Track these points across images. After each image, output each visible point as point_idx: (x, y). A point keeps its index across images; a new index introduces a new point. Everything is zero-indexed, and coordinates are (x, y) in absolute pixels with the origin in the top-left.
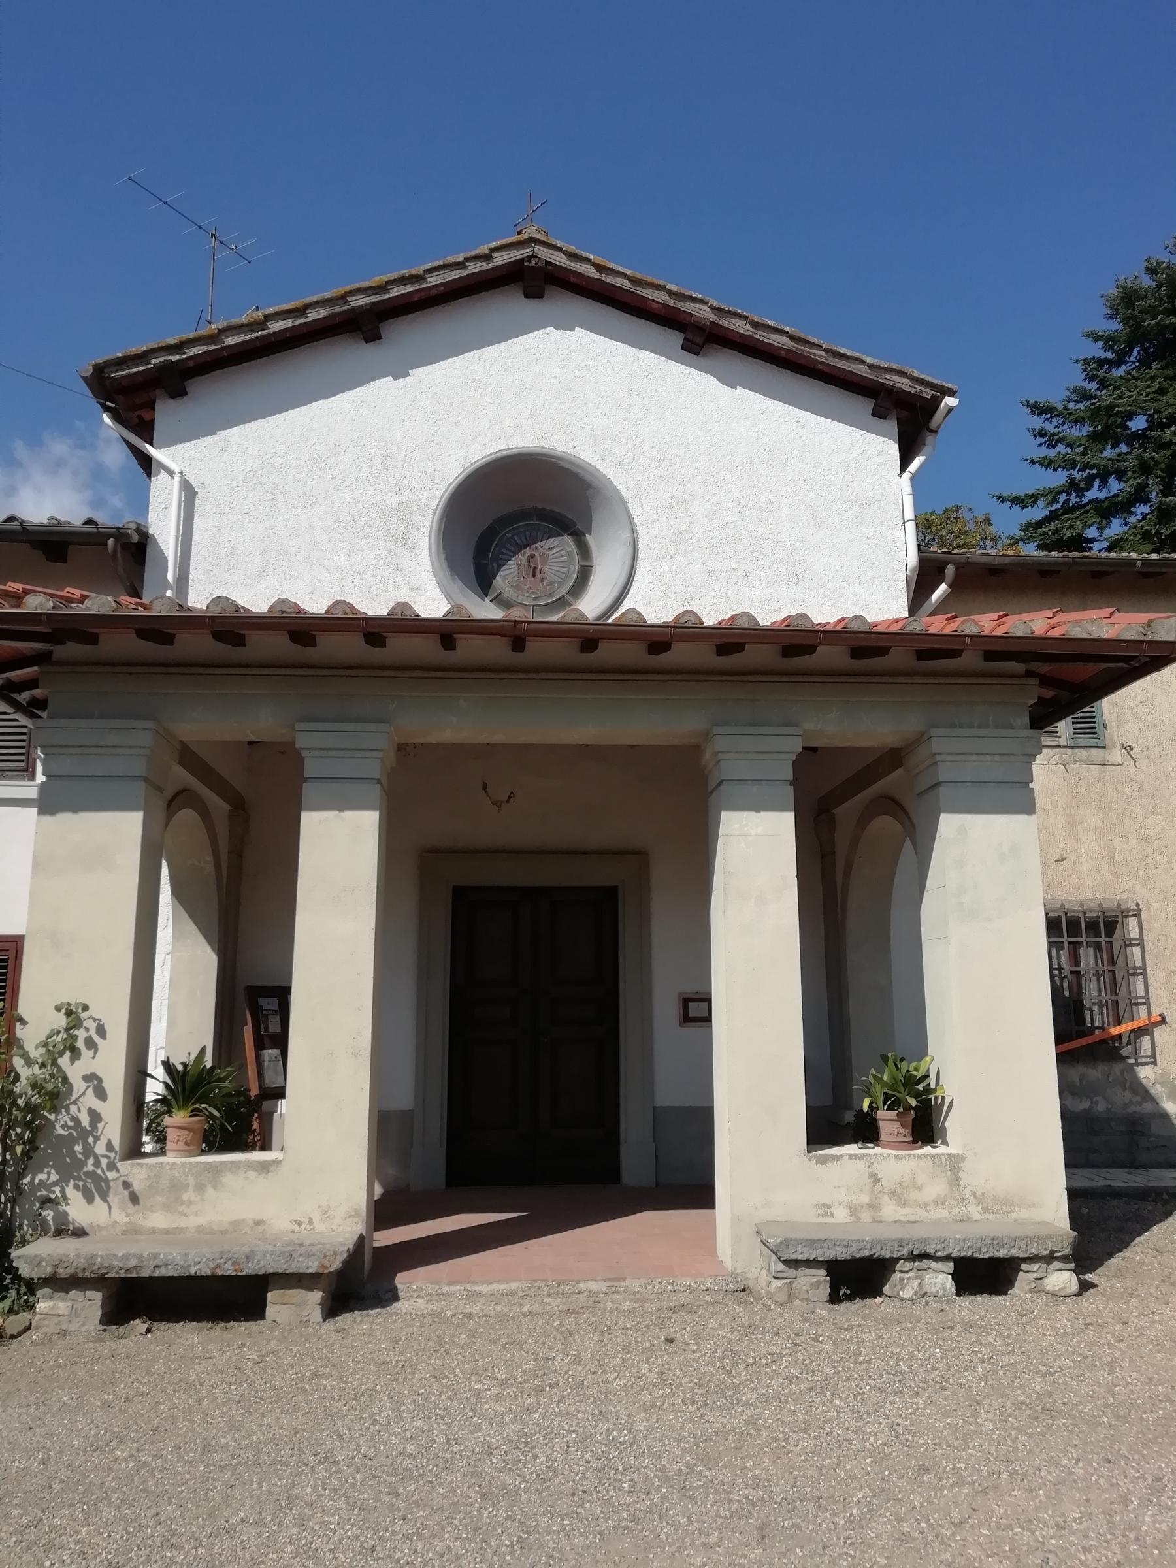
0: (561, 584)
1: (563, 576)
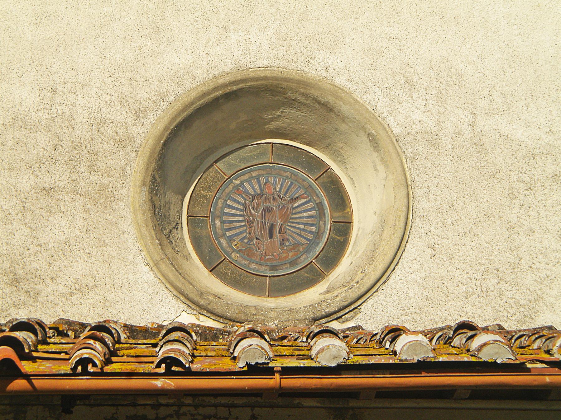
1: (310, 237)
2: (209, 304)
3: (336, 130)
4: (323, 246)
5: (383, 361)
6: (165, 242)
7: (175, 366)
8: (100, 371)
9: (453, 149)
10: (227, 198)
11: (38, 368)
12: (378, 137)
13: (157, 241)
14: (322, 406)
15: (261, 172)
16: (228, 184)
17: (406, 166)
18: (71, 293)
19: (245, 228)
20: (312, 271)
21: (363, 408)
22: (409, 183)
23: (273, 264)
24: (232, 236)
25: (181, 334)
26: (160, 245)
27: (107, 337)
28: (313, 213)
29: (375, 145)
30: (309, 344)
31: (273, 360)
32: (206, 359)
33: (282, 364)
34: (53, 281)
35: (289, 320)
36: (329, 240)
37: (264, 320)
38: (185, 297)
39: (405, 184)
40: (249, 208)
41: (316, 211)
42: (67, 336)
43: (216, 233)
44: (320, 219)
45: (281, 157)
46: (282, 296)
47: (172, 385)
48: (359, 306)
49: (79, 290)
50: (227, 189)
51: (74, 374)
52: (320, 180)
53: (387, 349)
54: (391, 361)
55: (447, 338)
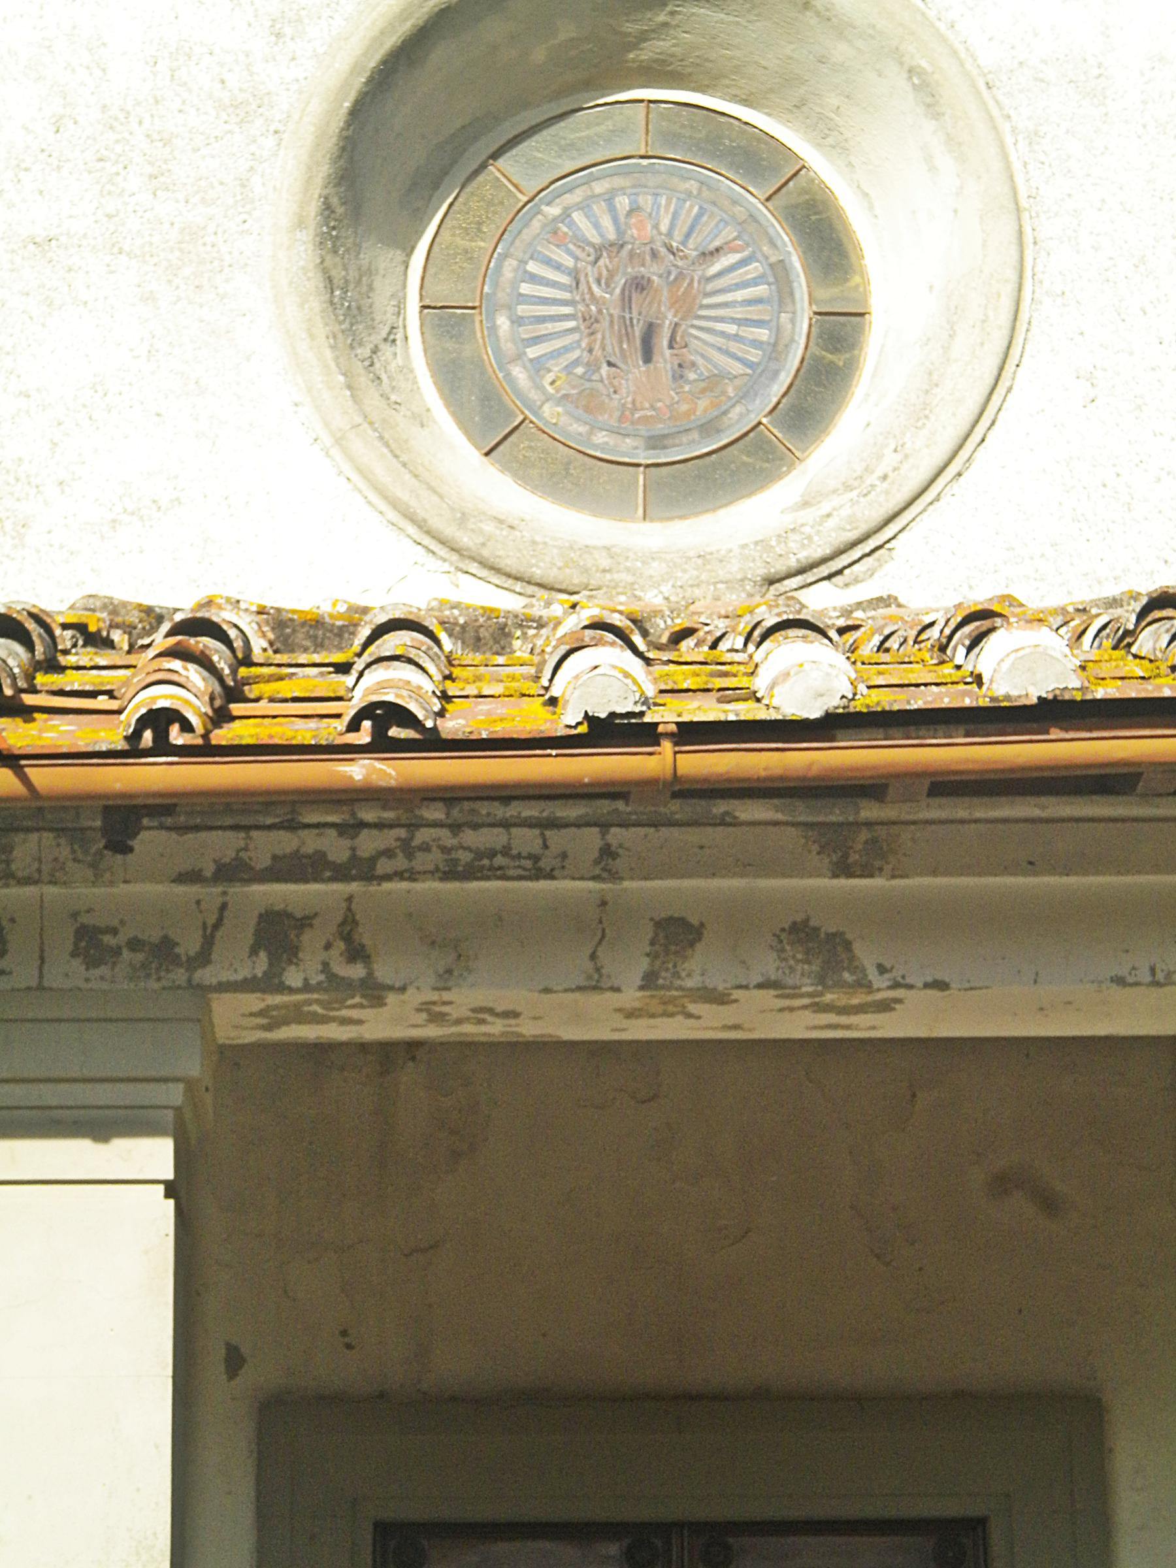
1: (755, 355)
2: (483, 544)
3: (821, 61)
4: (789, 381)
5: (946, 703)
6: (363, 379)
7: (398, 726)
8: (200, 741)
9: (1144, 102)
10: (527, 256)
11: (40, 738)
12: (936, 76)
13: (341, 378)
14: (790, 819)
15: (618, 182)
16: (528, 217)
17: (1013, 157)
18: (114, 521)
19: (576, 336)
20: (761, 448)
21: (894, 823)
22: (1024, 203)
23: (657, 433)
24: (544, 358)
25: (413, 639)
26: (349, 387)
27: (217, 651)
28: (761, 290)
29: (929, 100)
30: (751, 657)
31: (656, 704)
32: (480, 703)
33: (679, 716)
34: (63, 492)
35: (702, 582)
36: (805, 363)
37: (633, 584)
38: (420, 527)
39: (1012, 206)
40: (588, 282)
41: (769, 284)
42: (109, 644)
43: (498, 351)
44: (780, 306)
45: (671, 139)
46: (681, 517)
47: (390, 774)
48: (888, 541)
49: (133, 514)
50: (525, 231)
51: (132, 751)
52: (780, 200)
53: (958, 667)
54: (967, 702)
55: (1121, 632)
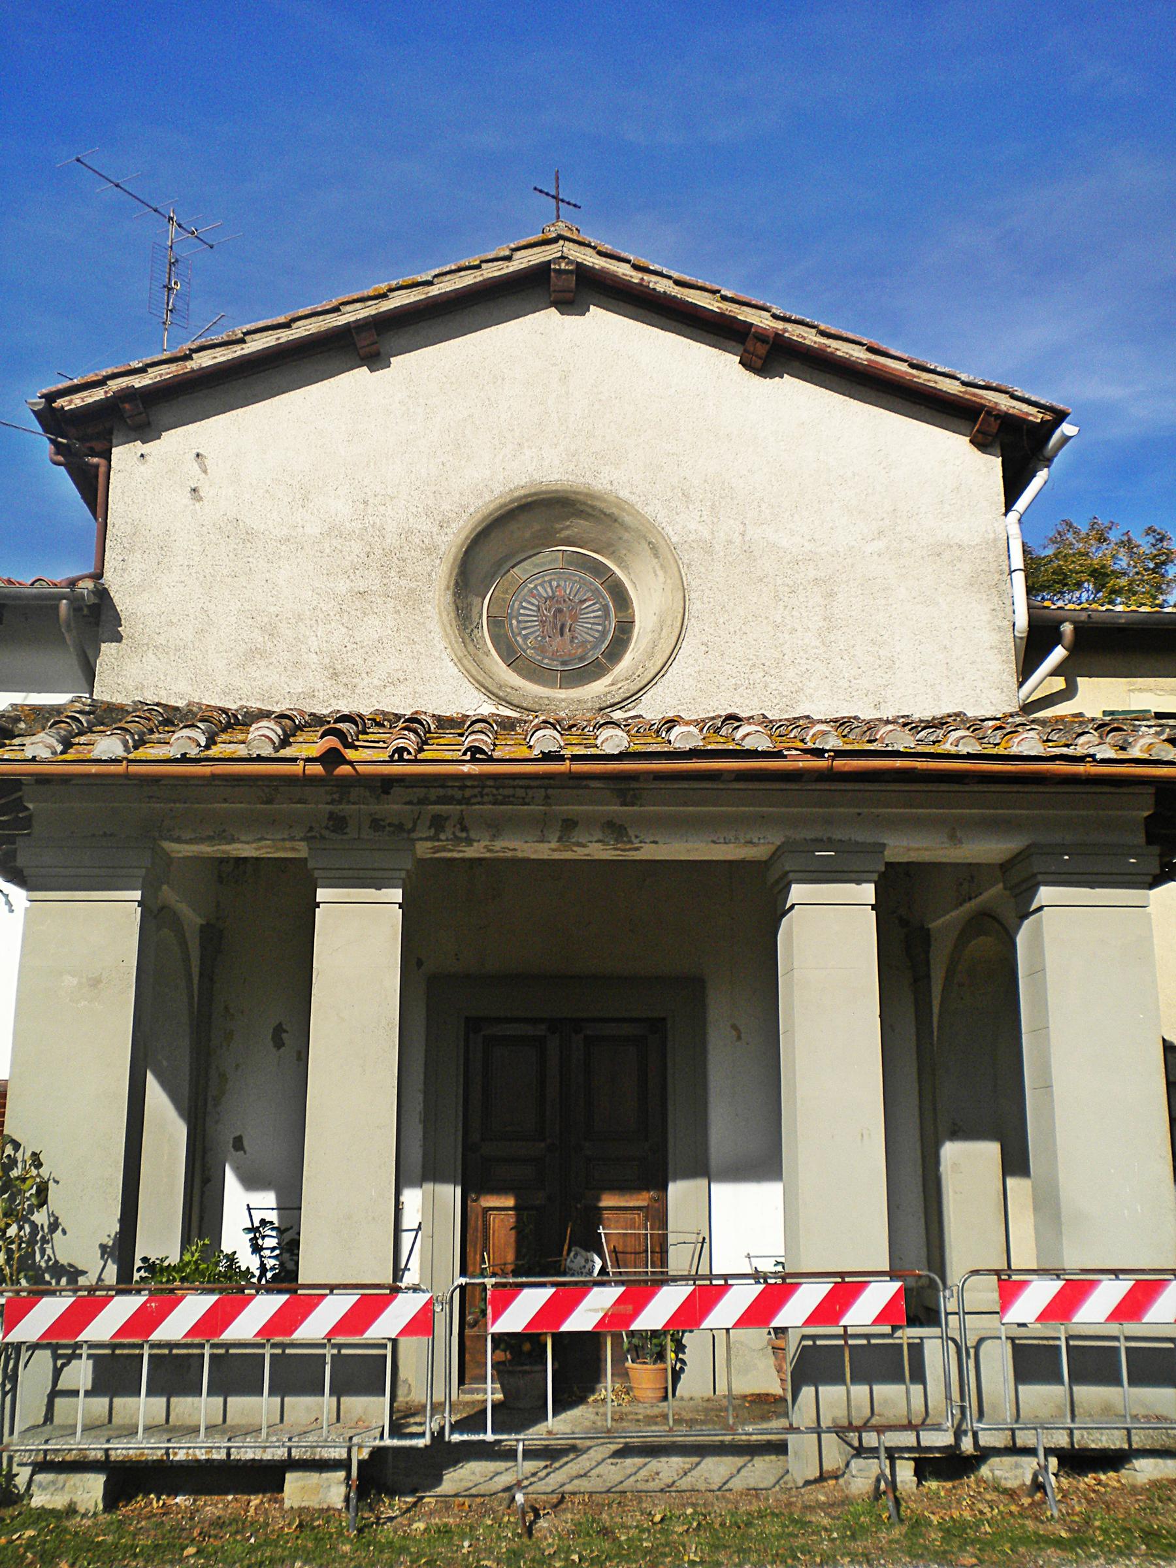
0: (594, 647)
